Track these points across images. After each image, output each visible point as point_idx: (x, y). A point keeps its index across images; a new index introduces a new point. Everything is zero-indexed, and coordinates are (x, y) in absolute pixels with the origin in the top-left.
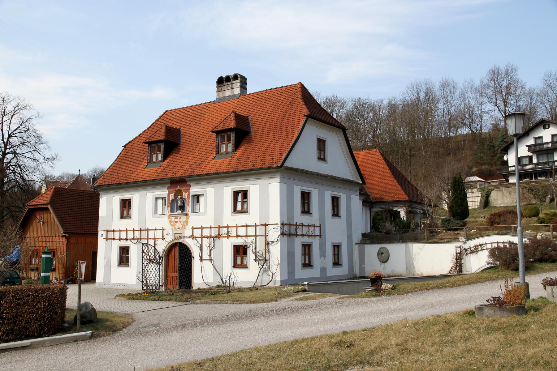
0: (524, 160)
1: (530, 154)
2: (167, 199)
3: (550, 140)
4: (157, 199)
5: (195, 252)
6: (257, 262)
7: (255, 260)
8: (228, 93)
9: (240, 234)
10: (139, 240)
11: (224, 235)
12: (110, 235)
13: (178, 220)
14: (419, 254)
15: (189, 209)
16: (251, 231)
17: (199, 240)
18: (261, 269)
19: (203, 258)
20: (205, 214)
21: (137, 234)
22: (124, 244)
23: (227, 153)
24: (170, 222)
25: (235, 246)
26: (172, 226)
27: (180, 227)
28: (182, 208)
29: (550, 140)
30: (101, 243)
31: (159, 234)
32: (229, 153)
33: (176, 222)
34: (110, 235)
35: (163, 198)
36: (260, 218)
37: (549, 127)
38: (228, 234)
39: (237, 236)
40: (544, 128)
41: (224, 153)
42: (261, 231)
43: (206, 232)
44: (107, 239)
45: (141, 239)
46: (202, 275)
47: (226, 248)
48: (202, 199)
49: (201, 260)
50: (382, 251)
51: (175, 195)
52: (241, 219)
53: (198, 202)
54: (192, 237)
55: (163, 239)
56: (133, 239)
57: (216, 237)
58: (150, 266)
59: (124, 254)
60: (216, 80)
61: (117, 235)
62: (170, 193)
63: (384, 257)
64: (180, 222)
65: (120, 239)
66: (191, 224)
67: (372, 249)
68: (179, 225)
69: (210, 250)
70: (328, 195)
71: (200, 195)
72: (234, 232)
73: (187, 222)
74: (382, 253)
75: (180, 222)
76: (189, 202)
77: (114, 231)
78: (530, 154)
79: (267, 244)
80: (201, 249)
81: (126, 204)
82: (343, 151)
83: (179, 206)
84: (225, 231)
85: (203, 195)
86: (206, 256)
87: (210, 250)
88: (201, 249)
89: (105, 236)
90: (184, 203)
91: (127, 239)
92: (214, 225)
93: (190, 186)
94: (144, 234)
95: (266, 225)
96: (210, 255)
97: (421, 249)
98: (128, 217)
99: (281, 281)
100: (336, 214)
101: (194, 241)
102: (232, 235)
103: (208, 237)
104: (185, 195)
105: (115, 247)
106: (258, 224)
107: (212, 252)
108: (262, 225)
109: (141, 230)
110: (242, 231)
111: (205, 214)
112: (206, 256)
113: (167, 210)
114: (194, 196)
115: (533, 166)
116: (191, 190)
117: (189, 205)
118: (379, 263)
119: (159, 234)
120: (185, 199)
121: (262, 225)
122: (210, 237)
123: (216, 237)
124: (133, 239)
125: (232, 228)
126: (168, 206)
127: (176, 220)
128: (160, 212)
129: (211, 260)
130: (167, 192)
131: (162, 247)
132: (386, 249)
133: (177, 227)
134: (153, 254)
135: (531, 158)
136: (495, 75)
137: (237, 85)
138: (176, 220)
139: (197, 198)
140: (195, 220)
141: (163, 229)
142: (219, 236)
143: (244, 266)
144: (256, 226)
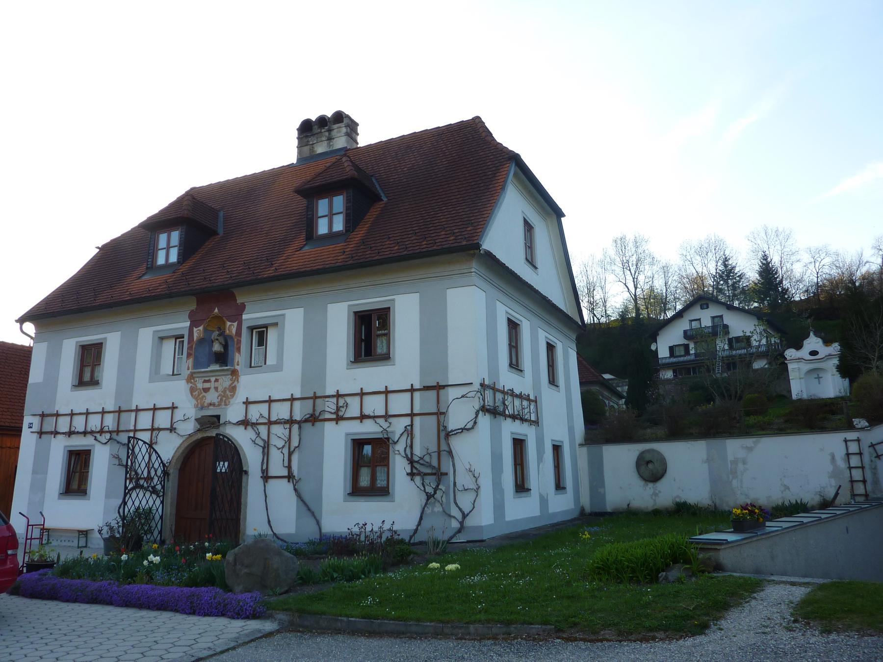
0: (677, 349)
1: (686, 342)
2: (186, 339)
3: (709, 324)
4: (162, 339)
5: (252, 457)
6: (418, 479)
7: (412, 475)
8: (320, 149)
9: (367, 411)
10: (114, 436)
11: (328, 416)
12: (49, 425)
13: (212, 385)
14: (744, 462)
15: (240, 359)
16: (400, 404)
17: (263, 430)
18: (429, 496)
19: (272, 473)
20: (278, 368)
21: (110, 421)
22: (79, 443)
23: (332, 236)
24: (192, 390)
25: (358, 444)
26: (196, 398)
27: (216, 401)
28: (222, 358)
29: (709, 324)
30: (28, 441)
31: (163, 419)
32: (338, 234)
33: (206, 390)
34: (49, 425)
35: (177, 337)
36: (423, 372)
37: (708, 307)
38: (336, 413)
39: (363, 417)
40: (702, 308)
41: (324, 237)
42: (423, 402)
43: (281, 411)
44: (41, 433)
45: (118, 432)
46: (269, 511)
47: (334, 443)
48: (272, 336)
49: (266, 477)
50: (648, 457)
51: (205, 329)
52: (372, 376)
53: (262, 341)
54: (245, 423)
55: (172, 429)
56: (101, 432)
57: (306, 421)
58: (134, 495)
59: (78, 465)
60: (298, 125)
61: (63, 425)
62: (194, 324)
63: (651, 470)
64: (216, 389)
65: (70, 433)
66: (242, 394)
67: (621, 457)
68: (212, 397)
69: (290, 454)
70: (543, 337)
71: (266, 327)
72: (353, 410)
73: (233, 389)
74: (648, 462)
75: (216, 389)
76: (239, 342)
77: (57, 415)
78: (686, 342)
79: (41, 539)
80: (266, 448)
81: (90, 357)
82: (554, 258)
83: (215, 354)
84: (330, 406)
85: (276, 324)
86: (277, 467)
87: (290, 454)
88: (266, 448)
89: (36, 428)
90: (226, 346)
91: (85, 433)
92: (302, 392)
93: (242, 308)
94: (129, 421)
95: (438, 388)
96: (289, 467)
97: (750, 449)
98: (94, 383)
99: (481, 527)
100: (553, 381)
101: (250, 433)
102: (346, 416)
103: (286, 422)
104: (231, 328)
105: (58, 449)
106: (417, 386)
107: (295, 458)
108: (427, 388)
109: (120, 411)
110: (374, 405)
111: (278, 368)
112: (277, 467)
113: (186, 366)
114: (251, 329)
115: (693, 357)
116: (244, 317)
117: (239, 350)
118: (642, 483)
119: (163, 419)
120: (231, 337)
121: (427, 388)
122: (291, 422)
123: (306, 421)
124: (101, 432)
125: (348, 399)
126: (189, 355)
127: (207, 385)
128: (167, 367)
129: (290, 477)
130: (188, 324)
131: (169, 448)
132: (659, 453)
133: (208, 401)
134: (147, 458)
135: (686, 347)
136: (621, 243)
137: (340, 131)
138: (207, 385)
139: (261, 333)
140: (252, 385)
141: (173, 408)
142: (313, 419)
143: (382, 492)
144: (412, 390)
